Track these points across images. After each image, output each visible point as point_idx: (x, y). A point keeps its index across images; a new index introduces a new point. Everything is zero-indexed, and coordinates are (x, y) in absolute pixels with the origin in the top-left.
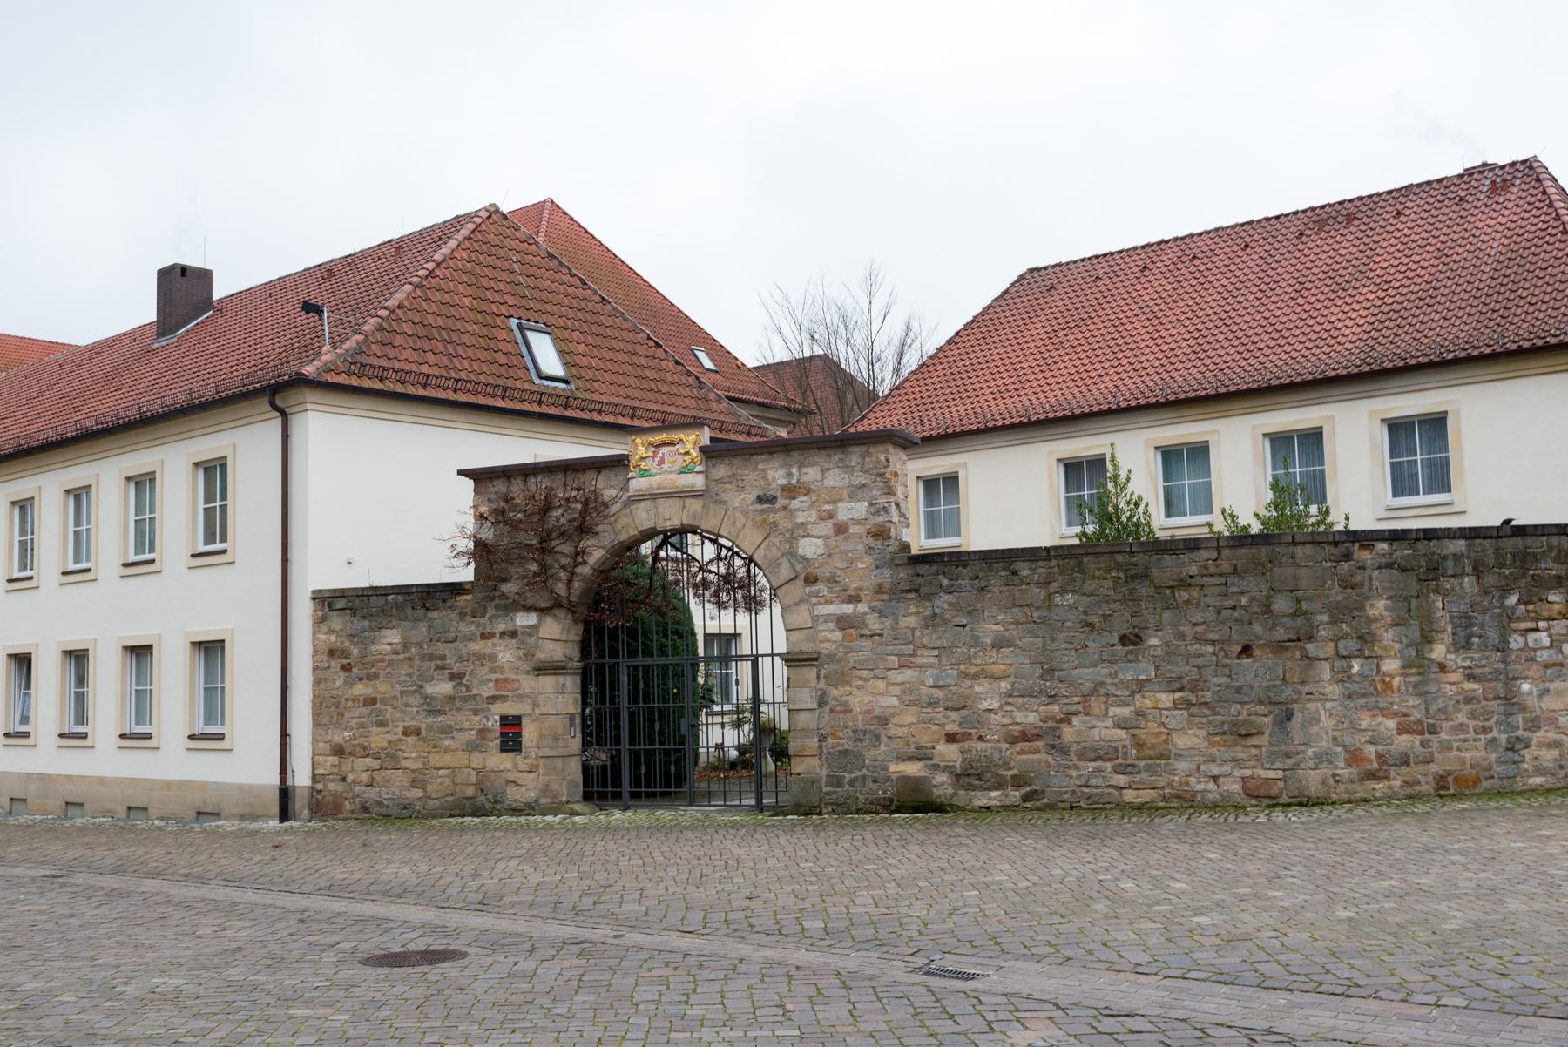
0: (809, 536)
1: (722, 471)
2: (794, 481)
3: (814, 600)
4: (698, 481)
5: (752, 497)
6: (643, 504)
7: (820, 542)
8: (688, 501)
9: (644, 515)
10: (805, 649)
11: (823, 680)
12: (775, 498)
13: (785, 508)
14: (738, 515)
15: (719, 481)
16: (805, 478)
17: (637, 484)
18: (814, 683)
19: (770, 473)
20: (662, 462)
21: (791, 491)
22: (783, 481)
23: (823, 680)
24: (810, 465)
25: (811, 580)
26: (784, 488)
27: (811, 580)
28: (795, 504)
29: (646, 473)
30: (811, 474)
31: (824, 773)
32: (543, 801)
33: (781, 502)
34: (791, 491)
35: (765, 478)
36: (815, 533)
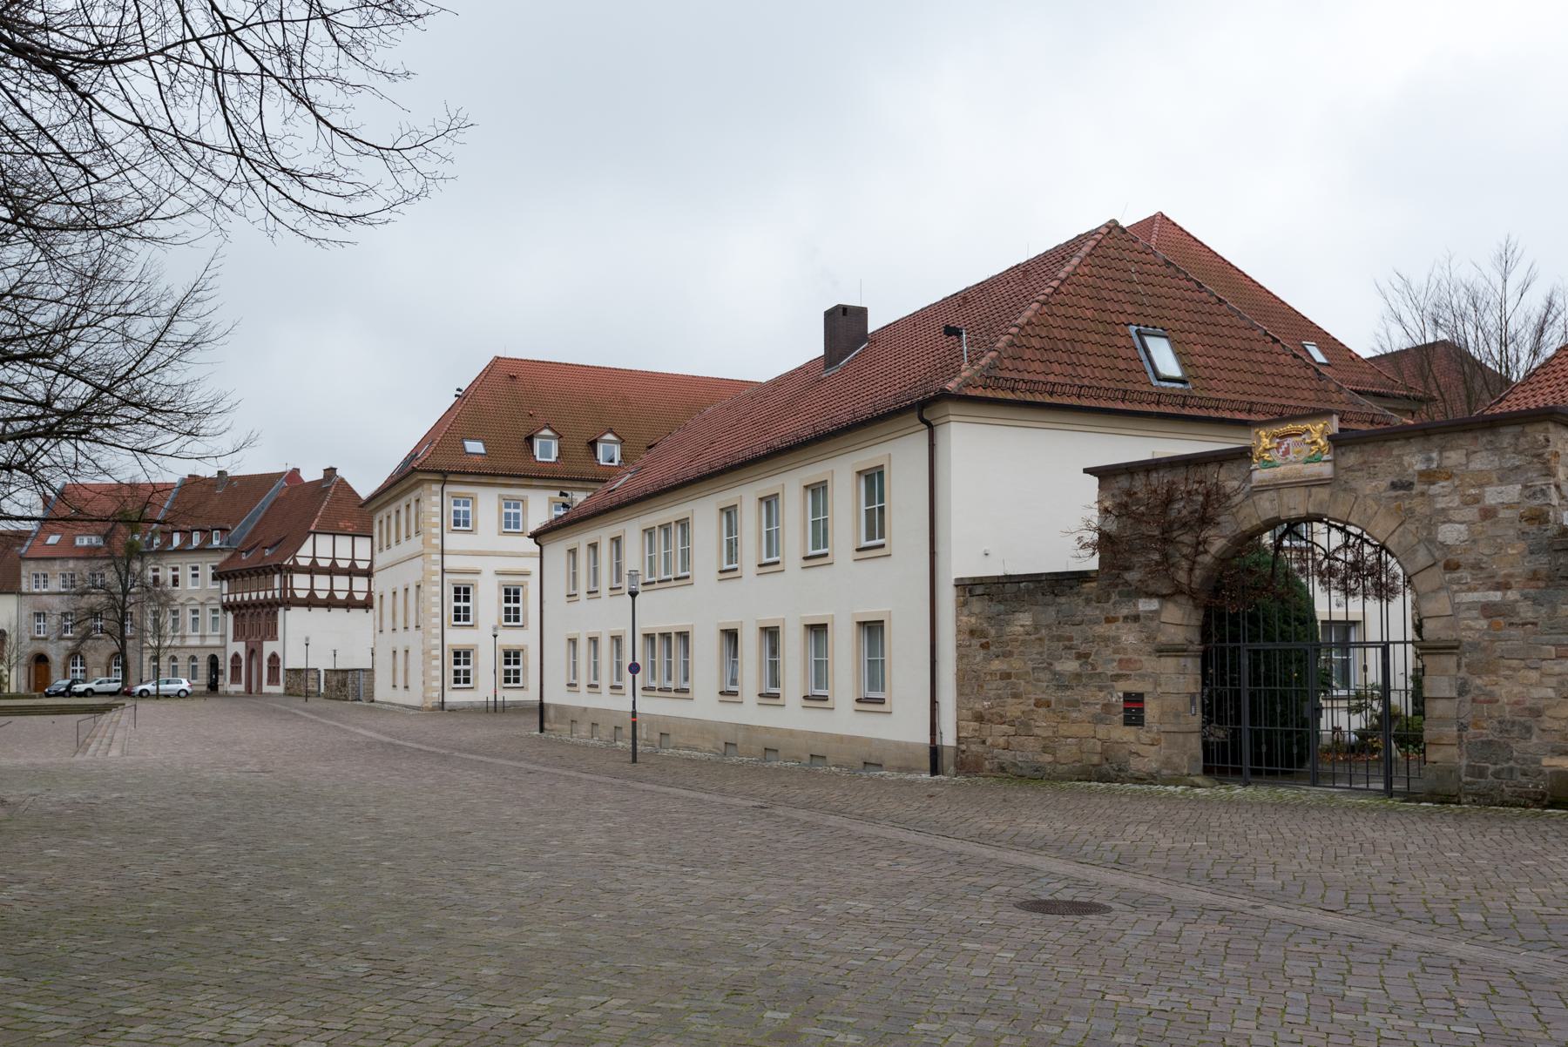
0: (1450, 521)
1: (1352, 458)
2: (1434, 466)
3: (1455, 587)
4: (1326, 470)
5: (1384, 483)
6: (1266, 495)
7: (1463, 527)
8: (1314, 490)
9: (1267, 505)
10: (1443, 637)
11: (1464, 669)
12: (1412, 484)
13: (1423, 494)
14: (1370, 502)
15: (1349, 469)
16: (1446, 463)
17: (1260, 475)
18: (1453, 671)
19: (1407, 459)
20: (1287, 452)
21: (1429, 477)
22: (1420, 467)
23: (1464, 669)
24: (1452, 449)
25: (1451, 567)
26: (1421, 474)
27: (1451, 567)
28: (1435, 489)
29: (1270, 464)
30: (1454, 457)
31: (1464, 762)
32: (1165, 772)
33: (1418, 488)
34: (1429, 477)
35: (1401, 464)
36: (1457, 518)
